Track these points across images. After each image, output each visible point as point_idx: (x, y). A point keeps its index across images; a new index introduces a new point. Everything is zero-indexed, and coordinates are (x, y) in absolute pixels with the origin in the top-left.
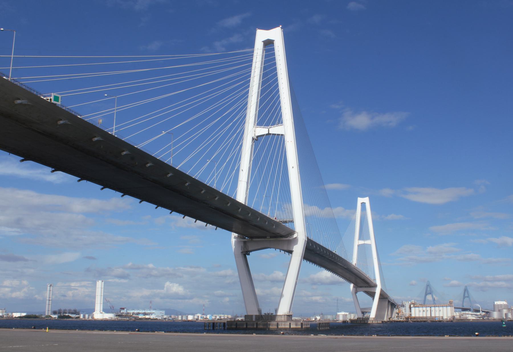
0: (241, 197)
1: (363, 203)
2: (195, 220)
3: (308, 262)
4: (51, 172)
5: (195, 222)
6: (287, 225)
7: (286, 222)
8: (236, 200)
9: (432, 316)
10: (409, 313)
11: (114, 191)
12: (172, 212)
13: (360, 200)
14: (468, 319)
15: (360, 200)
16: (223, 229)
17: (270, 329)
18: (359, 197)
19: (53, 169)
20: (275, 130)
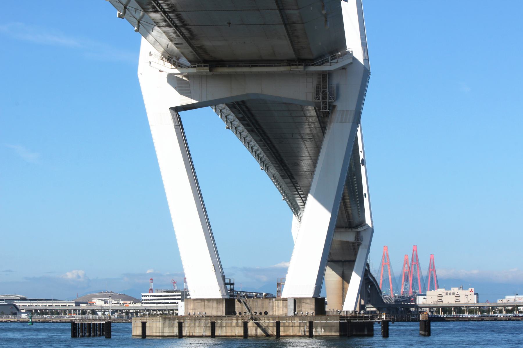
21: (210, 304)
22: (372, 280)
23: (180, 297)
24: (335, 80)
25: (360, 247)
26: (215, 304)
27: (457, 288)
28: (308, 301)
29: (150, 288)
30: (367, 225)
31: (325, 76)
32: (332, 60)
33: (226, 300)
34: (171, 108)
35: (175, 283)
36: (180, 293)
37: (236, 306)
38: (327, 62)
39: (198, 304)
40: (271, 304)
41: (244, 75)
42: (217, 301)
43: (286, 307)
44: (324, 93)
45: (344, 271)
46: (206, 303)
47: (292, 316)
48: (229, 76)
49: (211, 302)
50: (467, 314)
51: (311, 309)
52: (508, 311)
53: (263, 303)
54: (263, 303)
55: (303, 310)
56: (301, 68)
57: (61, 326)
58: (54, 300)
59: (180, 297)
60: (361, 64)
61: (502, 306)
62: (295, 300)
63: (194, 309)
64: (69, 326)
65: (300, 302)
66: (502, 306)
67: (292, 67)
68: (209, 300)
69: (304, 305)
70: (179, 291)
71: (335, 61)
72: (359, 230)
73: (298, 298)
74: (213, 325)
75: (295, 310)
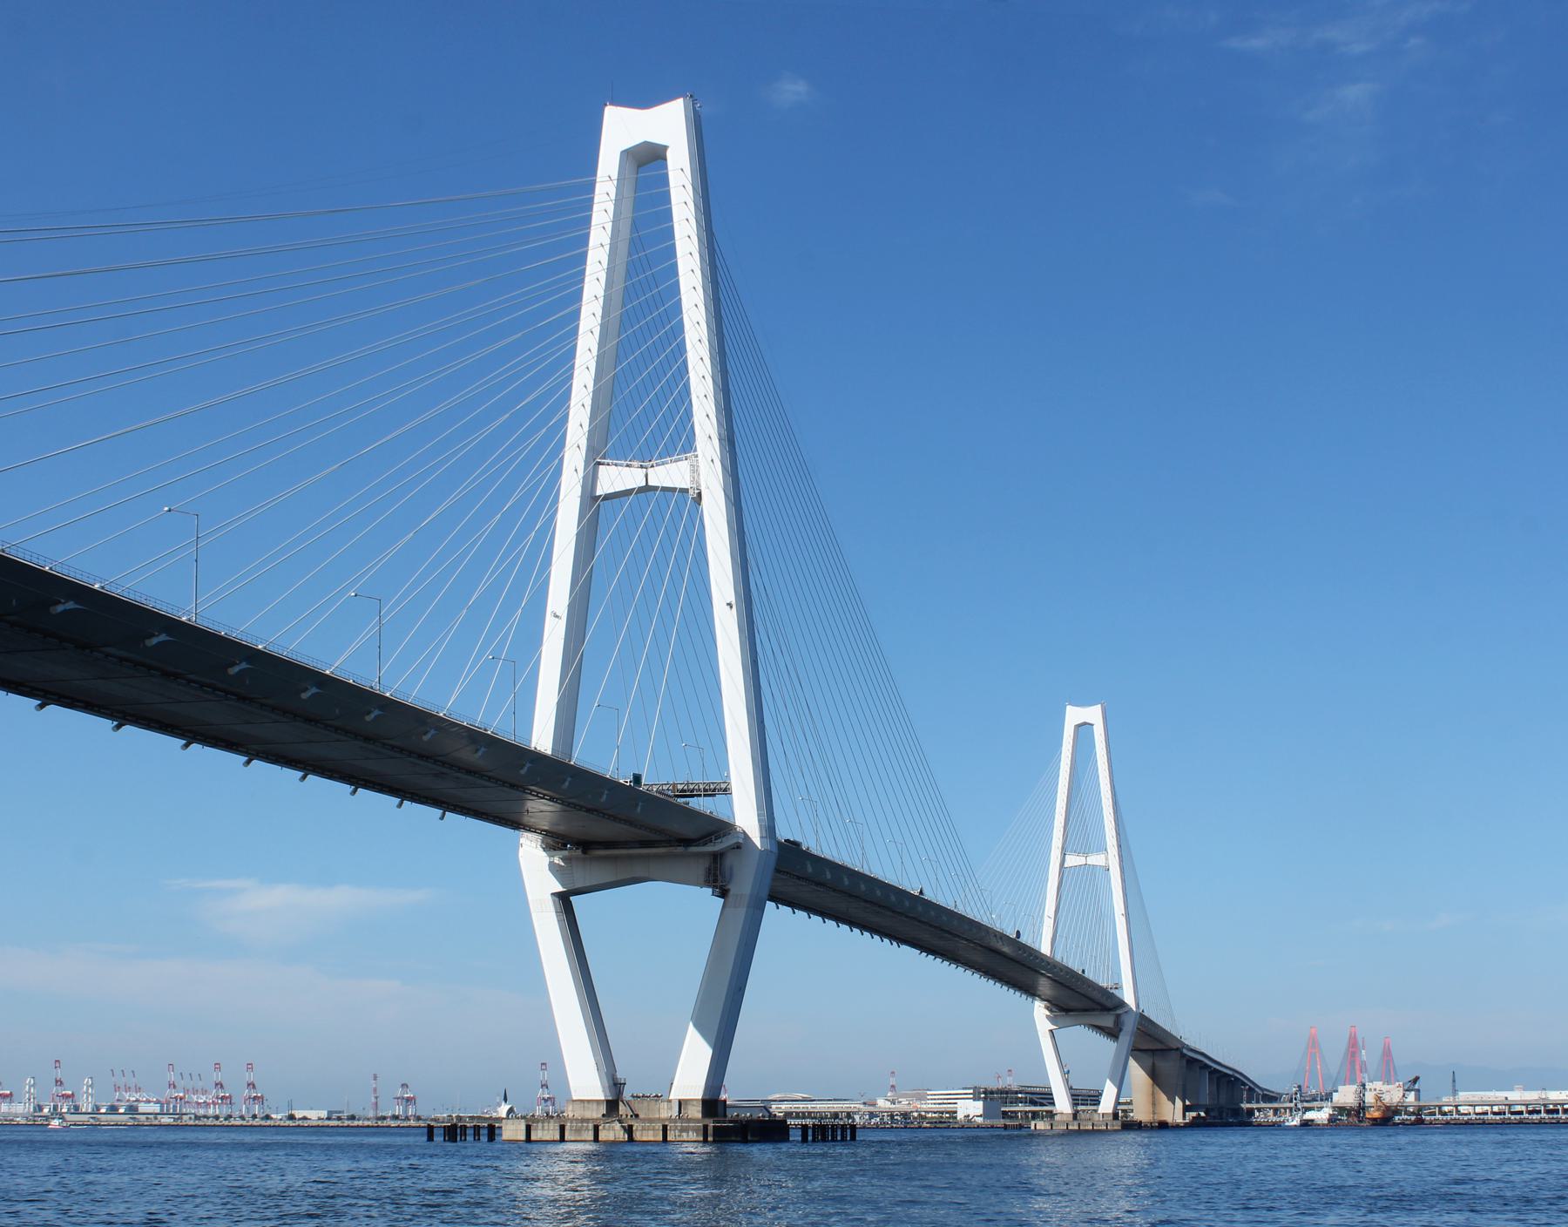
0: (1045, 949)
1: (1085, 724)
2: (397, 800)
3: (886, 941)
4: (37, 710)
5: (442, 818)
6: (700, 804)
7: (684, 794)
8: (1042, 951)
9: (650, 484)
10: (77, 1103)
11: (287, 777)
12: (192, 745)
13: (1074, 715)
14: (1051, 1011)
15: (1074, 715)
16: (284, 769)
17: (1521, 1086)
18: (612, 104)
19: (115, 723)
20: (1096, 860)
21: (590, 1106)
22: (1230, 1073)
23: (971, 1096)
24: (729, 861)
25: (1122, 1033)
26: (595, 1105)
27: (1381, 1083)
28: (695, 1103)
29: (891, 1084)
30: (1128, 1005)
31: (717, 857)
32: (716, 839)
33: (608, 1101)
34: (552, 894)
35: (999, 1077)
36: (971, 1091)
37: (620, 1108)
38: (711, 842)
39: (577, 1106)
40: (658, 1106)
41: (630, 857)
42: (598, 1102)
43: (670, 1108)
44: (716, 875)
45: (1156, 1062)
46: (586, 1104)
47: (1324, 1125)
48: (616, 858)
49: (591, 1103)
50: (1543, 1115)
51: (698, 1112)
52: (1548, 1112)
53: (648, 1105)
54: (648, 1105)
55: (689, 1112)
56: (680, 849)
57: (420, 1131)
58: (845, 1100)
59: (971, 1096)
60: (756, 846)
61: (1505, 1105)
62: (680, 1102)
63: (573, 1111)
64: (426, 1130)
65: (686, 1104)
66: (1505, 1105)
67: (671, 848)
68: (589, 1101)
69: (690, 1107)
70: (969, 1088)
71: (719, 840)
72: (1118, 1012)
73: (683, 1100)
74: (665, 1128)
75: (680, 1112)
